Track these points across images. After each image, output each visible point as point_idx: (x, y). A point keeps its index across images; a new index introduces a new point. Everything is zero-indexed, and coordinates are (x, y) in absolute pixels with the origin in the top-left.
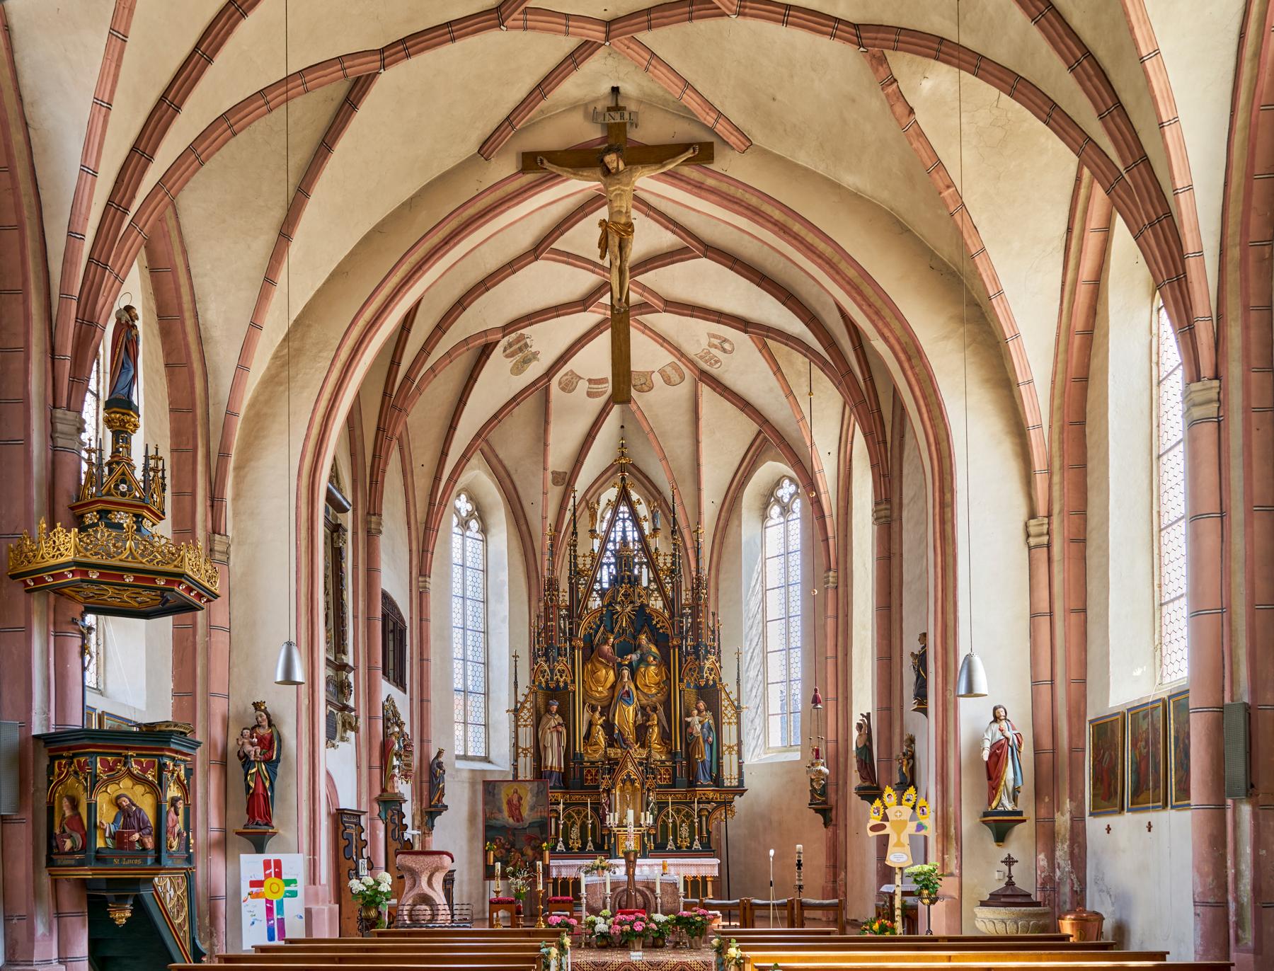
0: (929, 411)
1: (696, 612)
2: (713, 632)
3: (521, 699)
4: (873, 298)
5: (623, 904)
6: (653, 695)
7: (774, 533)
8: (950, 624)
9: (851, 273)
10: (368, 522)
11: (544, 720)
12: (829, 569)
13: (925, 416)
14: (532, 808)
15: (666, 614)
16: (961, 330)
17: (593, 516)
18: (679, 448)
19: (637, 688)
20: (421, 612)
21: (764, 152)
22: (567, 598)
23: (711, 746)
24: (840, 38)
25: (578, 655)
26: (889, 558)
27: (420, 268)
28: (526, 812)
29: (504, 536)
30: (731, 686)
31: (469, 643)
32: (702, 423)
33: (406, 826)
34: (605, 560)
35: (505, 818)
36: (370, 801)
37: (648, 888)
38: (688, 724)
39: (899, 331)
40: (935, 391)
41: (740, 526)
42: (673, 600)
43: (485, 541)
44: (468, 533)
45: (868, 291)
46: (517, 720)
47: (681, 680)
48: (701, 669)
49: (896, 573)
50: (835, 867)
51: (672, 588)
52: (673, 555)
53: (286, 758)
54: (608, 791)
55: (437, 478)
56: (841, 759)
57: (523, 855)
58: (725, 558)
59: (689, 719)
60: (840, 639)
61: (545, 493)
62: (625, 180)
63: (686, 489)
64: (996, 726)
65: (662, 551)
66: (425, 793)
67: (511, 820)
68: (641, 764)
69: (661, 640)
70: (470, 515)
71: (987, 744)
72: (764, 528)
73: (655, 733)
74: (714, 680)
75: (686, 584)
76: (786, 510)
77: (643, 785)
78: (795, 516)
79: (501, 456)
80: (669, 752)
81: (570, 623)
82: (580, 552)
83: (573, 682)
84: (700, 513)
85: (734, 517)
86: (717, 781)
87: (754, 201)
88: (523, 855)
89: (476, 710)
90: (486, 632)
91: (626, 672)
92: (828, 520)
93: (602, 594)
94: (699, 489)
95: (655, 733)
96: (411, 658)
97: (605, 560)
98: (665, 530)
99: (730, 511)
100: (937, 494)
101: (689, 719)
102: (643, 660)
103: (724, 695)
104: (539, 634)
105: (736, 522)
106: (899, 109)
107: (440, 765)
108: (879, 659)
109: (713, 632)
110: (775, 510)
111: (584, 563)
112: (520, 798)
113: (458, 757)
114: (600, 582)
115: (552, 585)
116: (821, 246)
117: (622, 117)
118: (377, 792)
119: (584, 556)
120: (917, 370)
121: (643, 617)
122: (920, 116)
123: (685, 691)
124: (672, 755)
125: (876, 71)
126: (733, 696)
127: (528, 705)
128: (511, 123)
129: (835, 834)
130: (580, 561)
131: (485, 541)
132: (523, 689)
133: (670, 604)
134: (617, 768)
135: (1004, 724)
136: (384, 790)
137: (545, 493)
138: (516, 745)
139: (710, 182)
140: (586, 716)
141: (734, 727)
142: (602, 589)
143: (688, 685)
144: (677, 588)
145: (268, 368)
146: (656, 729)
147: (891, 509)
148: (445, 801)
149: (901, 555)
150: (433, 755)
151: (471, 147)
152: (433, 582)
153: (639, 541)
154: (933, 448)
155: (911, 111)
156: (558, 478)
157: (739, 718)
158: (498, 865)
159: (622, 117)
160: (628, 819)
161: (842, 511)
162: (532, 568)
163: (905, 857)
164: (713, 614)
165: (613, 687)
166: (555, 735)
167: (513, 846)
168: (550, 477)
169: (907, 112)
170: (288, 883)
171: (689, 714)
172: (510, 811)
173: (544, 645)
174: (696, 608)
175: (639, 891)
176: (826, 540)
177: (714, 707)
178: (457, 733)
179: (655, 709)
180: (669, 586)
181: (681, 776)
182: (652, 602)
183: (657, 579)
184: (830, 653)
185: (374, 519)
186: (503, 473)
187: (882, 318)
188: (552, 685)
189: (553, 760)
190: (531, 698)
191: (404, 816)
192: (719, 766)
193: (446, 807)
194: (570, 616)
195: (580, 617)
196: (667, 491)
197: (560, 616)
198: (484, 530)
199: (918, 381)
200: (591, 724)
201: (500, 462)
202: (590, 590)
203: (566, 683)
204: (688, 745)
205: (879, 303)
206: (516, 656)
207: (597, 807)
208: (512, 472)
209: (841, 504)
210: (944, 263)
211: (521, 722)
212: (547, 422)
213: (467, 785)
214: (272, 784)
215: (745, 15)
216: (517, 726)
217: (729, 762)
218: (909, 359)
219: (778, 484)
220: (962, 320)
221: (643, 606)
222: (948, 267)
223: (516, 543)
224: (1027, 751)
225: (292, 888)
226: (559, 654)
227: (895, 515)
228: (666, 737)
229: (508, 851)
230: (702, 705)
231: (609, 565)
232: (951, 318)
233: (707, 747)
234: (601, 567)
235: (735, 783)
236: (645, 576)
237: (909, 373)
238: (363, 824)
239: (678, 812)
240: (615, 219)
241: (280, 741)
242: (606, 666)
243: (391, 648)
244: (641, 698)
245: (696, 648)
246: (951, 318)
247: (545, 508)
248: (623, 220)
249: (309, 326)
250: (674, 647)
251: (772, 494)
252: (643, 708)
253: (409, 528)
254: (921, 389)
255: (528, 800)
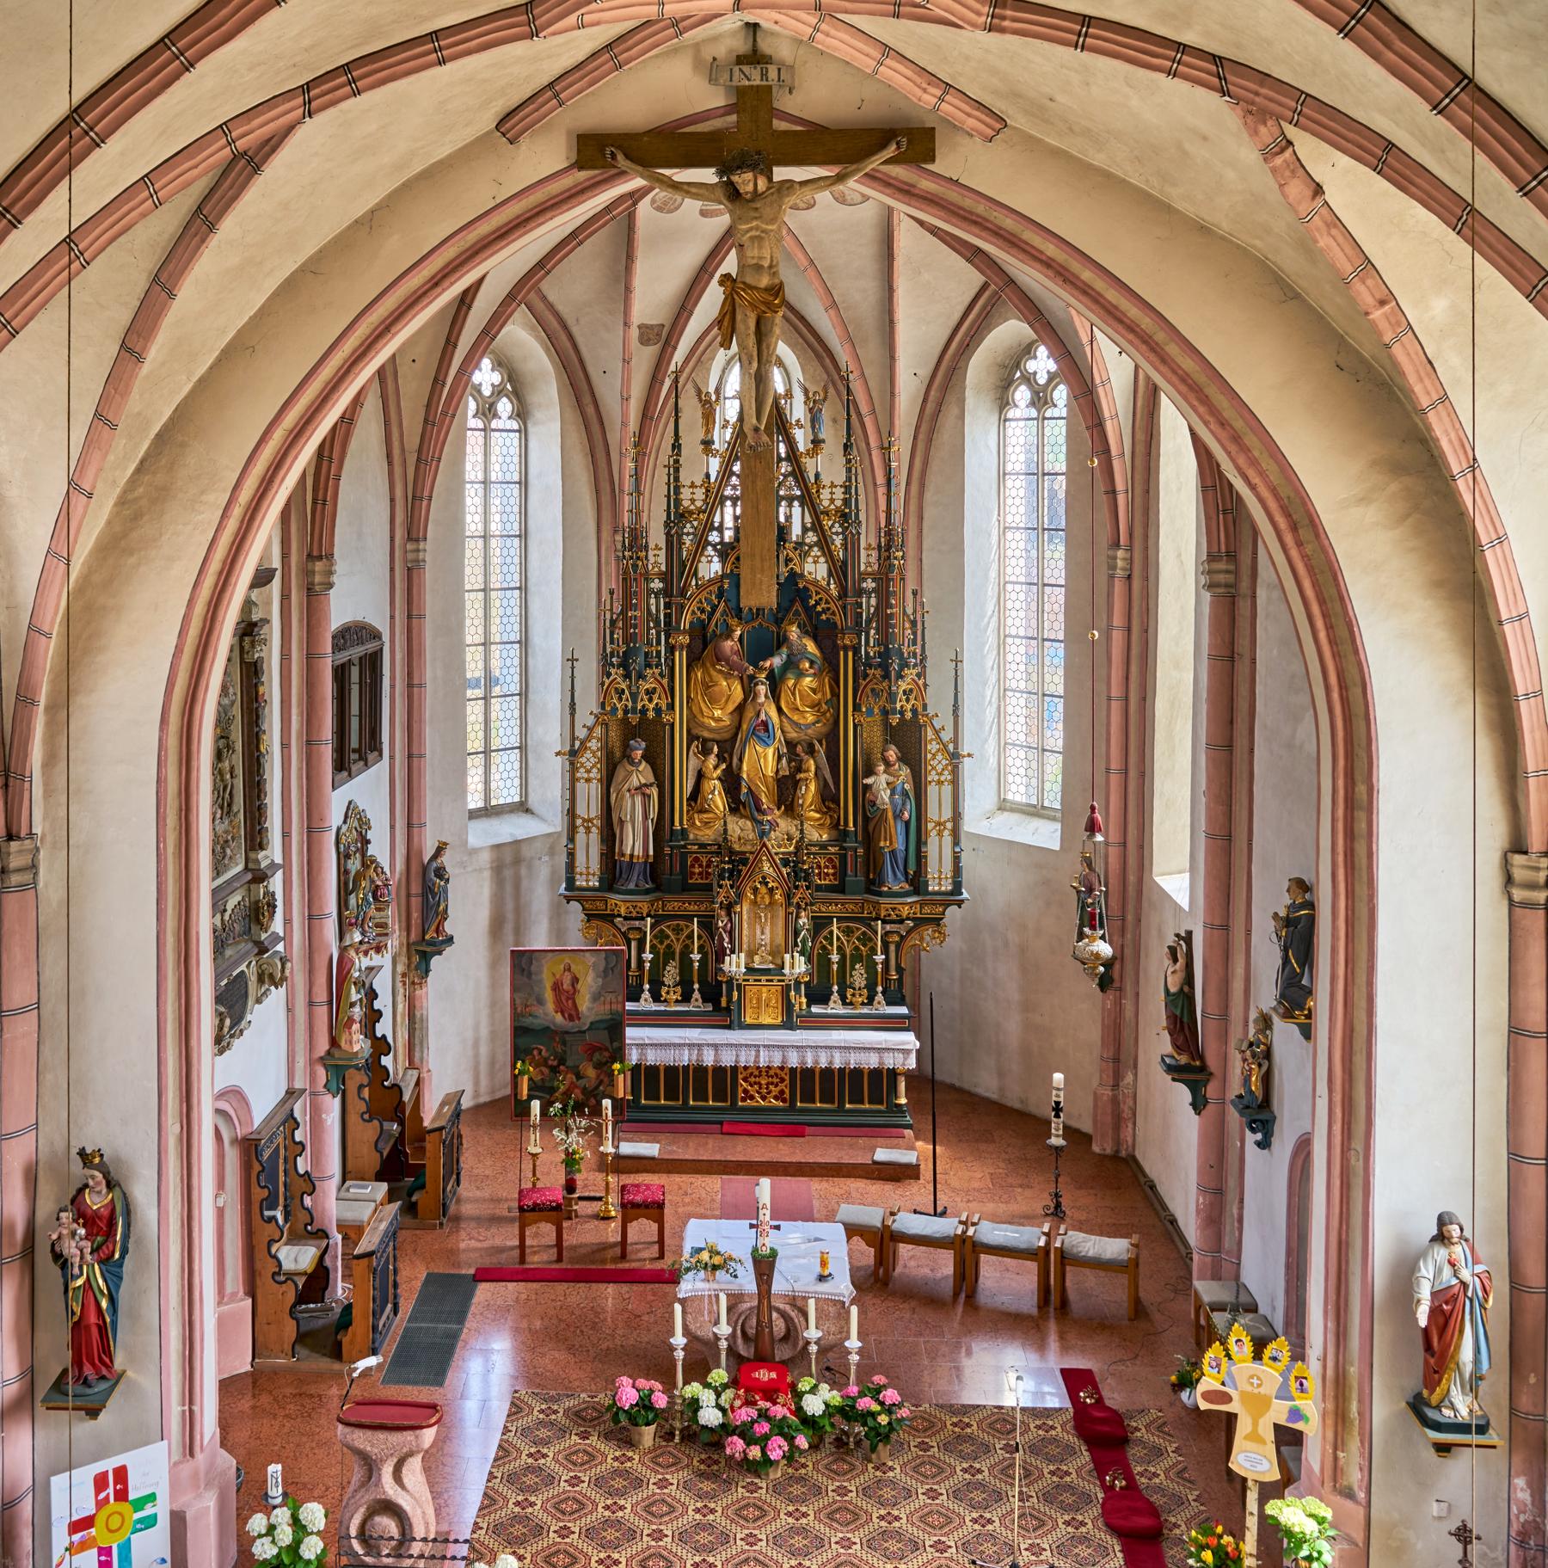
0: (1329, 627)
1: (884, 594)
2: (914, 623)
3: (581, 733)
4: (1229, 413)
5: (751, 1332)
6: (808, 726)
7: (1019, 433)
8: (1360, 1029)
9: (1188, 364)
10: (307, 573)
11: (620, 773)
12: (1116, 544)
13: (1322, 635)
14: (596, 998)
15: (835, 593)
16: (1394, 487)
17: (708, 417)
18: (859, 292)
19: (780, 710)
20: (409, 602)
21: (1031, 143)
22: (662, 559)
23: (907, 824)
24: (1186, 78)
25: (681, 658)
26: (1232, 659)
27: (388, 329)
28: (584, 1004)
29: (556, 426)
30: (944, 720)
31: (494, 560)
32: (899, 263)
33: (379, 1014)
34: (728, 492)
35: (549, 1013)
36: (312, 1063)
37: (794, 1305)
38: (867, 787)
39: (1275, 477)
40: (1342, 599)
41: (962, 402)
42: (844, 563)
43: (524, 432)
44: (494, 424)
45: (1212, 391)
46: (573, 768)
47: (856, 708)
48: (892, 697)
49: (1242, 690)
50: (1117, 1060)
51: (845, 545)
52: (847, 489)
53: (139, 1242)
54: (729, 908)
55: (438, 382)
56: (1132, 878)
57: (579, 1076)
58: (935, 465)
59: (869, 781)
60: (1134, 669)
61: (626, 361)
62: (768, 212)
63: (871, 352)
64: (1441, 1253)
65: (826, 480)
66: (415, 915)
67: (559, 1018)
68: (786, 863)
69: (821, 631)
70: (498, 392)
71: (1425, 1293)
72: (1003, 421)
73: (809, 792)
74: (914, 711)
75: (867, 538)
76: (1041, 399)
77: (788, 897)
78: (1055, 412)
79: (551, 298)
80: (835, 826)
81: (668, 605)
82: (685, 478)
83: (671, 707)
84: (892, 394)
85: (951, 398)
86: (917, 883)
87: (1008, 223)
88: (579, 1076)
89: (507, 749)
90: (524, 589)
91: (762, 689)
92: (1116, 464)
93: (725, 551)
94: (892, 358)
95: (809, 792)
96: (393, 687)
97: (728, 492)
98: (831, 435)
99: (945, 388)
100: (1341, 783)
101: (869, 781)
102: (791, 664)
103: (930, 734)
104: (613, 622)
105: (955, 411)
106: (1297, 189)
107: (440, 873)
108: (1210, 836)
109: (914, 623)
110: (1022, 394)
111: (693, 498)
112: (575, 980)
113: (474, 815)
114: (720, 529)
115: (636, 541)
116: (1133, 312)
117: (764, 75)
118: (323, 1045)
119: (693, 486)
120: (1309, 549)
121: (793, 590)
122: (1331, 195)
123: (862, 729)
124: (841, 836)
125: (1254, 133)
126: (947, 736)
127: (594, 744)
128: (556, 95)
129: (1119, 1004)
130: (686, 494)
131: (524, 432)
132: (585, 717)
133: (839, 570)
134: (744, 869)
135: (1458, 1251)
136: (334, 1042)
137: (626, 361)
138: (571, 813)
139: (926, 185)
140: (694, 763)
141: (947, 789)
142: (722, 543)
143: (870, 712)
144: (851, 544)
145: (109, 523)
146: (812, 787)
147: (1236, 573)
148: (448, 927)
149: (1253, 661)
150: (428, 853)
151: (488, 120)
152: (431, 550)
153: (788, 459)
154: (1336, 695)
155: (1318, 190)
156: (648, 334)
157: (955, 771)
158: (536, 1105)
159: (764, 75)
160: (758, 937)
161: (1140, 448)
162: (604, 475)
163: (1265, 1466)
164: (915, 593)
165: (740, 709)
166: (638, 800)
167: (562, 1061)
168: (634, 333)
169: (1309, 193)
170: (140, 1504)
171: (870, 772)
172: (558, 1001)
173: (623, 655)
174: (885, 576)
175: (778, 1310)
176: (1113, 492)
177: (913, 758)
178: (471, 719)
179: (811, 751)
180: (838, 540)
181: (855, 877)
182: (809, 567)
183: (817, 527)
184: (1116, 692)
185: (319, 566)
186: (555, 324)
187: (1245, 449)
188: (634, 719)
189: (635, 843)
190: (598, 731)
191: (376, 996)
192: (921, 859)
193: (450, 940)
194: (667, 592)
195: (683, 593)
196: (843, 355)
197: (650, 591)
198: (522, 414)
199: (1310, 569)
200: (700, 776)
201: (551, 307)
202: (701, 543)
203: (658, 710)
204: (866, 820)
205: (1238, 424)
206: (573, 660)
207: (708, 925)
208: (570, 322)
209: (1140, 436)
210: (1363, 360)
211: (581, 773)
212: (630, 258)
213: (487, 874)
214: (112, 1300)
215: (1002, 30)
216: (573, 780)
217: (938, 852)
218: (1294, 528)
219: (1028, 351)
220: (1396, 468)
221: (794, 577)
222: (1369, 367)
223: (577, 438)
224: (1498, 1301)
225: (148, 1511)
226: (649, 666)
227: (1245, 585)
228: (828, 799)
229: (555, 1070)
230: (892, 754)
231: (734, 500)
232: (1374, 463)
233: (900, 827)
234: (722, 504)
235: (947, 886)
236: (796, 518)
237: (1294, 553)
238: (297, 1114)
239: (848, 932)
240: (749, 280)
241: (128, 1213)
242: (727, 676)
243: (355, 709)
244: (788, 728)
245: (885, 655)
246: (1374, 463)
247: (626, 382)
248: (764, 281)
249: (183, 445)
250: (846, 648)
251: (1018, 366)
252: (791, 745)
253: (390, 463)
254: (1315, 584)
255: (589, 982)
